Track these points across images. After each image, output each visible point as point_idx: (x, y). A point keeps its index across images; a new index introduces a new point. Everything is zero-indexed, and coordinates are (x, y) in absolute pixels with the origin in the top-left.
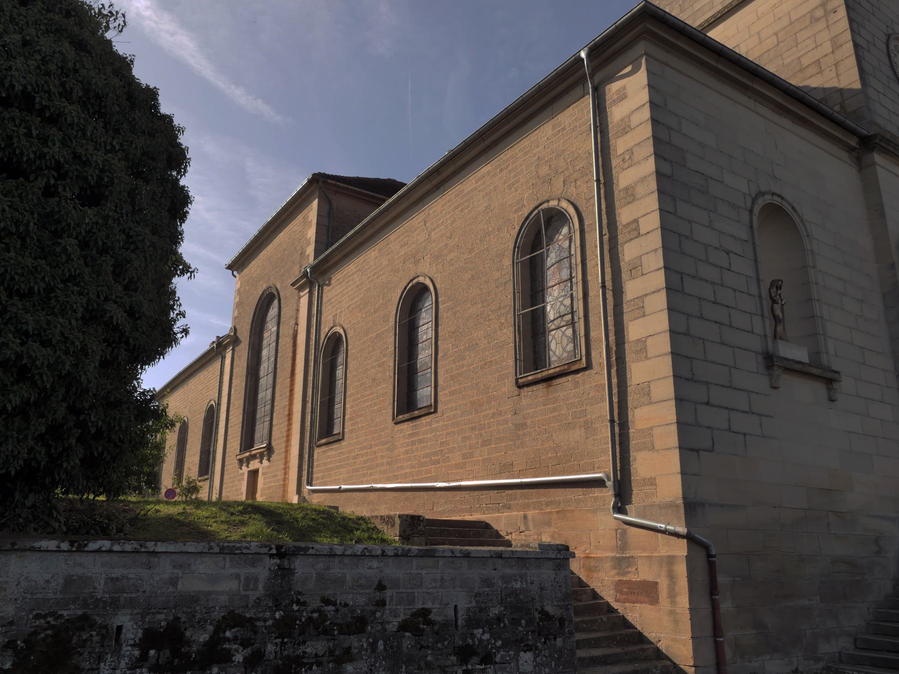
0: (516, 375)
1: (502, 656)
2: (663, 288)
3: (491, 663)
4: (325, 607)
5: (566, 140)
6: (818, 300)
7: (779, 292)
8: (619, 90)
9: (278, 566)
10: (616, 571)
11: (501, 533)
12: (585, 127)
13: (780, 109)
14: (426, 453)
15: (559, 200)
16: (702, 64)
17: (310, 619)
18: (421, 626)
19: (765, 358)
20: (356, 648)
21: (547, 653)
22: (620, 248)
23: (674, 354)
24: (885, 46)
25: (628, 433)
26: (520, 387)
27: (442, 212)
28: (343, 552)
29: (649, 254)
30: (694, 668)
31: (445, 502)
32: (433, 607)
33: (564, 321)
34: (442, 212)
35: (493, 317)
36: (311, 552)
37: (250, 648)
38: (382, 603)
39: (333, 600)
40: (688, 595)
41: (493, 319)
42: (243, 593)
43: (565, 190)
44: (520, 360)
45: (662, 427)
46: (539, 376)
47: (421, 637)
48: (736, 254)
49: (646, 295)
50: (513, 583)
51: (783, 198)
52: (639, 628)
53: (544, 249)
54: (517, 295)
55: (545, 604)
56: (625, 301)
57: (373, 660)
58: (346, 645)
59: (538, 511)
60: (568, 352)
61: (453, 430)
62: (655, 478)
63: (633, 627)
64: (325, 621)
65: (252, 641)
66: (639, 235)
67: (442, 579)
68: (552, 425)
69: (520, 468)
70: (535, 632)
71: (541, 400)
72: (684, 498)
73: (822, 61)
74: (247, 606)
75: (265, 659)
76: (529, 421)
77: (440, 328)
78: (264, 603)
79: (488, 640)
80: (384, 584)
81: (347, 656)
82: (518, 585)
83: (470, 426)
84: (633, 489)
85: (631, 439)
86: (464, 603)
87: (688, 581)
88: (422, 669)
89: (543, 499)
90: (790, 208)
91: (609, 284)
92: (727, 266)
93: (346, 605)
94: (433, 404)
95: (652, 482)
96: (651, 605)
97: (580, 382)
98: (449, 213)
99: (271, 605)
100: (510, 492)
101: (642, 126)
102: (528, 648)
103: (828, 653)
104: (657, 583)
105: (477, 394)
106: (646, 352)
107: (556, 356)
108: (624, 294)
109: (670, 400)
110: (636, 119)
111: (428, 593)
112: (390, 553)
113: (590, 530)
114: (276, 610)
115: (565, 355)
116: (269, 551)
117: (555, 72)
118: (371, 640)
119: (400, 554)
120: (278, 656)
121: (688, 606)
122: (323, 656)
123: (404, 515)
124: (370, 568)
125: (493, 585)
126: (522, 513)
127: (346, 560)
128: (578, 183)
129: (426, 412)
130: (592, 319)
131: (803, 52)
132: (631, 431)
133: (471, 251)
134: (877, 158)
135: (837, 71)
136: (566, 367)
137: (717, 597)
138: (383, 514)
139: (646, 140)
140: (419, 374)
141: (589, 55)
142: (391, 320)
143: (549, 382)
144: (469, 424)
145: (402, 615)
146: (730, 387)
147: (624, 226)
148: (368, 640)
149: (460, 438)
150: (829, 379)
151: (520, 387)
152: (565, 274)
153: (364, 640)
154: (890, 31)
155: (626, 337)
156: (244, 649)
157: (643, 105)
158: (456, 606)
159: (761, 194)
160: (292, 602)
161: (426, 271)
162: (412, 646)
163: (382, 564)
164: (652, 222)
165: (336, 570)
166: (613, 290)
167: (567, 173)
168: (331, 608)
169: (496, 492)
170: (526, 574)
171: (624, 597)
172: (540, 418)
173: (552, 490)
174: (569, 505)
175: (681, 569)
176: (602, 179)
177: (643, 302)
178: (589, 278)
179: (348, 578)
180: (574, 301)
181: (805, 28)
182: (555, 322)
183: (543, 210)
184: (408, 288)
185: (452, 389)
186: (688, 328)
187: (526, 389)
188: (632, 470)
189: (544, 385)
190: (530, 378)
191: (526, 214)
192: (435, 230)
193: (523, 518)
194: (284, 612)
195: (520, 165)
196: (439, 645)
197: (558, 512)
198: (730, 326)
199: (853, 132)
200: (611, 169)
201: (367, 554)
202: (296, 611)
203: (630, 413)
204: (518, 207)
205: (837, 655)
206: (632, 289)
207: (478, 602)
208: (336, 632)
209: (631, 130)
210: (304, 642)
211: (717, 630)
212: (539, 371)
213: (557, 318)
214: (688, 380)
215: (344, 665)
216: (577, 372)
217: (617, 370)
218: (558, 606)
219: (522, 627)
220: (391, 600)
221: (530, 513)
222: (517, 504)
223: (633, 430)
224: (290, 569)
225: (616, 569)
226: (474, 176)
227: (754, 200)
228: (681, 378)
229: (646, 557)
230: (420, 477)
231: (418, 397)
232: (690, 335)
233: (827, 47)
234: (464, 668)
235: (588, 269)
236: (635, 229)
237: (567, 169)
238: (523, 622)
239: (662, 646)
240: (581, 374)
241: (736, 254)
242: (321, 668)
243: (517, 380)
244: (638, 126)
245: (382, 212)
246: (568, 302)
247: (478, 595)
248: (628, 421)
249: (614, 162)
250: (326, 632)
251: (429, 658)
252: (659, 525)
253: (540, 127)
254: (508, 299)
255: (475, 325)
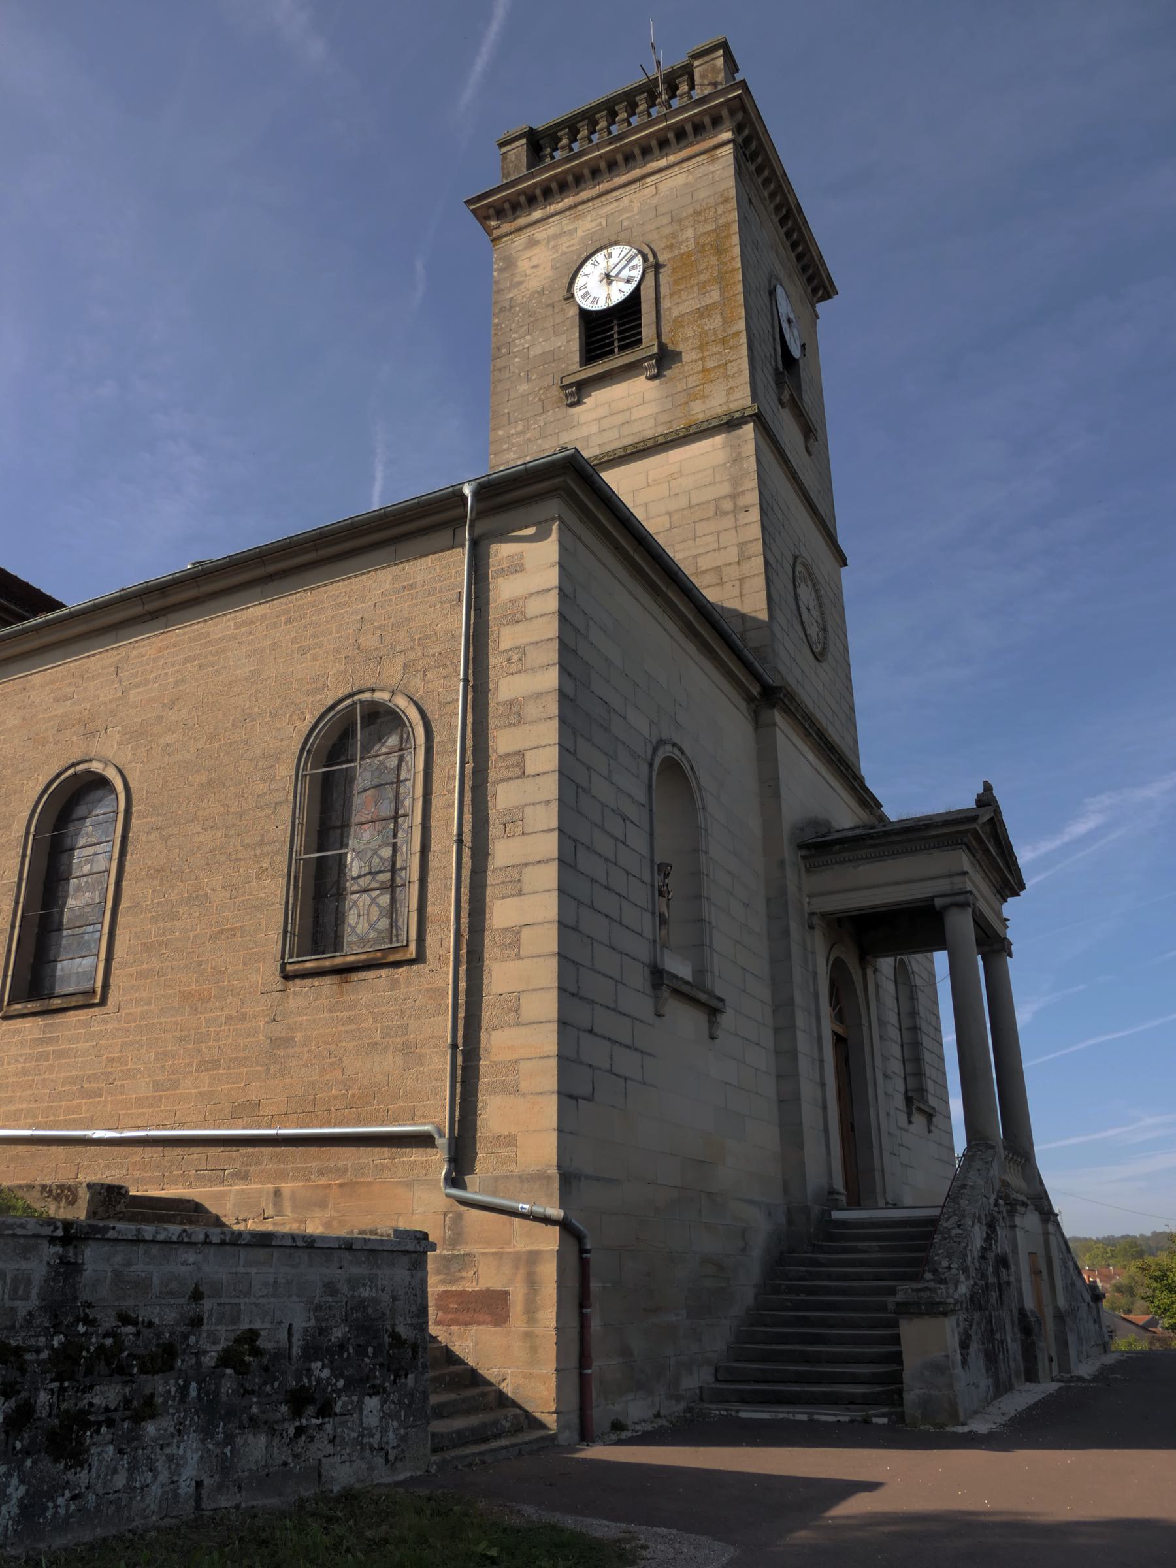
0: (283, 958)
1: (344, 1403)
2: (554, 859)
3: (330, 1416)
4: (122, 1328)
5: (415, 605)
6: (708, 899)
7: (667, 881)
8: (512, 556)
9: (60, 1258)
10: (440, 1277)
11: (224, 1219)
12: (453, 595)
13: (690, 631)
14: (72, 1077)
15: (393, 693)
16: (617, 548)
17: (101, 1347)
18: (247, 1358)
19: (652, 973)
20: (162, 1396)
21: (394, 1397)
22: (490, 789)
23: (561, 956)
24: (791, 570)
25: (478, 1066)
26: (287, 977)
27: (155, 660)
28: (154, 1237)
29: (538, 806)
30: (555, 1415)
31: (107, 1166)
32: (263, 1327)
33: (378, 881)
34: (155, 660)
35: (247, 856)
36: (111, 1234)
37: (13, 1400)
38: (196, 1322)
39: (133, 1315)
40: (555, 1308)
41: (245, 859)
42: (8, 1303)
43: (405, 681)
44: (293, 934)
45: (534, 1061)
46: (327, 963)
47: (245, 1377)
48: (632, 822)
49: (526, 865)
50: (362, 1290)
51: (683, 752)
52: (472, 1363)
53: (357, 764)
54: (298, 827)
55: (397, 1322)
56: (490, 868)
57: (182, 1415)
58: (147, 1392)
59: (302, 1184)
60: (379, 932)
61: (137, 1038)
62: (516, 1136)
63: (459, 1361)
64: (121, 1351)
65: (18, 1387)
66: (523, 775)
67: (276, 1282)
68: (344, 1044)
69: (275, 1111)
70: (383, 1365)
71: (326, 1002)
72: (559, 1167)
73: (723, 569)
74: (13, 1327)
75: (35, 1417)
76: (299, 1036)
77: (128, 857)
78: (38, 1321)
79: (328, 1379)
80: (201, 1290)
81: (147, 1409)
82: (365, 1293)
83: (177, 1034)
84: (479, 1151)
85: (481, 1075)
86: (301, 1321)
87: (558, 1288)
88: (244, 1428)
89: (314, 1164)
90: (689, 768)
91: (467, 838)
92: (622, 838)
93: (150, 1324)
94: (99, 990)
95: (510, 1141)
96: (495, 1325)
97: (401, 980)
98: (173, 665)
99: (47, 1325)
100: (250, 1150)
101: (544, 618)
102: (375, 1391)
103: (690, 1389)
104: (507, 1293)
105: (197, 981)
106: (519, 948)
107: (357, 934)
108: (490, 858)
109: (550, 1022)
110: (534, 607)
111: (256, 1305)
112: (215, 1240)
113: (399, 1215)
114: (55, 1333)
115: (373, 935)
116: (53, 1232)
117: (416, 500)
118: (181, 1382)
119: (228, 1241)
120: (55, 1411)
121: (554, 1324)
122: (116, 1410)
123: (98, 1184)
124: (185, 1263)
125: (337, 1291)
126: (270, 1186)
127: (155, 1250)
128: (429, 675)
129: (81, 1003)
130: (432, 886)
131: (701, 551)
132: (482, 1063)
133: (211, 738)
134: (778, 717)
135: (741, 589)
136: (379, 954)
137: (588, 1310)
138: (49, 1182)
139: (548, 640)
140: (65, 933)
141: (476, 494)
142: (15, 827)
143: (344, 976)
144: (176, 1030)
145: (222, 1340)
146: (615, 1010)
147: (501, 756)
148: (177, 1382)
149: (153, 1054)
150: (712, 1010)
151: (287, 977)
152: (386, 809)
153: (172, 1382)
154: (797, 553)
155: (487, 922)
156: (5, 1401)
157: (549, 590)
158: (290, 1325)
159: (661, 742)
160: (78, 1320)
161: (110, 754)
162: (233, 1391)
163: (200, 1258)
164: (545, 759)
165: (140, 1267)
166: (472, 848)
167: (411, 655)
168: (130, 1329)
169: (220, 1149)
170: (377, 1275)
171: (450, 1316)
172: (321, 1031)
173: (333, 1150)
174: (363, 1175)
175: (549, 1271)
176: (471, 678)
177: (520, 874)
178: (433, 823)
179: (156, 1280)
180: (399, 854)
181: (708, 519)
182: (361, 881)
183: (361, 702)
184: (63, 777)
185: (145, 966)
186: (577, 921)
187: (298, 982)
188: (479, 1122)
189: (336, 979)
190: (309, 965)
191: (330, 703)
192: (137, 686)
193: (272, 1195)
194: (66, 1336)
195: (327, 622)
196: (268, 1388)
197: (341, 1185)
198: (621, 923)
199: (757, 677)
200: (488, 669)
201: (186, 1240)
202: (82, 1335)
203: (483, 1036)
204: (314, 686)
205: (698, 1391)
206: (503, 852)
207: (317, 1319)
208: (135, 1370)
209: (527, 619)
210: (91, 1387)
211: (584, 1359)
212: (328, 955)
213: (365, 875)
214: (573, 995)
215: (143, 1424)
216: (397, 964)
217: (468, 970)
218: (411, 1325)
219: (369, 1357)
220: (211, 1315)
221: (287, 1187)
222: (261, 1172)
223: (487, 1063)
224: (76, 1263)
225: (440, 1274)
226: (232, 615)
227: (655, 751)
228: (566, 991)
229: (493, 1254)
230: (52, 1118)
231: (59, 973)
232: (580, 932)
233: (732, 554)
234: (297, 1424)
235: (433, 809)
236: (518, 765)
237: (412, 649)
238: (370, 1350)
239: (507, 1388)
240: (404, 968)
241: (632, 822)
242: (112, 1431)
243: (283, 966)
244: (537, 617)
245: (24, 632)
246: (387, 852)
247: (318, 1307)
248: (479, 1048)
249: (493, 660)
250: (122, 1370)
251: (255, 1410)
252: (521, 1205)
253: (370, 572)
254: (282, 832)
255: (207, 864)
